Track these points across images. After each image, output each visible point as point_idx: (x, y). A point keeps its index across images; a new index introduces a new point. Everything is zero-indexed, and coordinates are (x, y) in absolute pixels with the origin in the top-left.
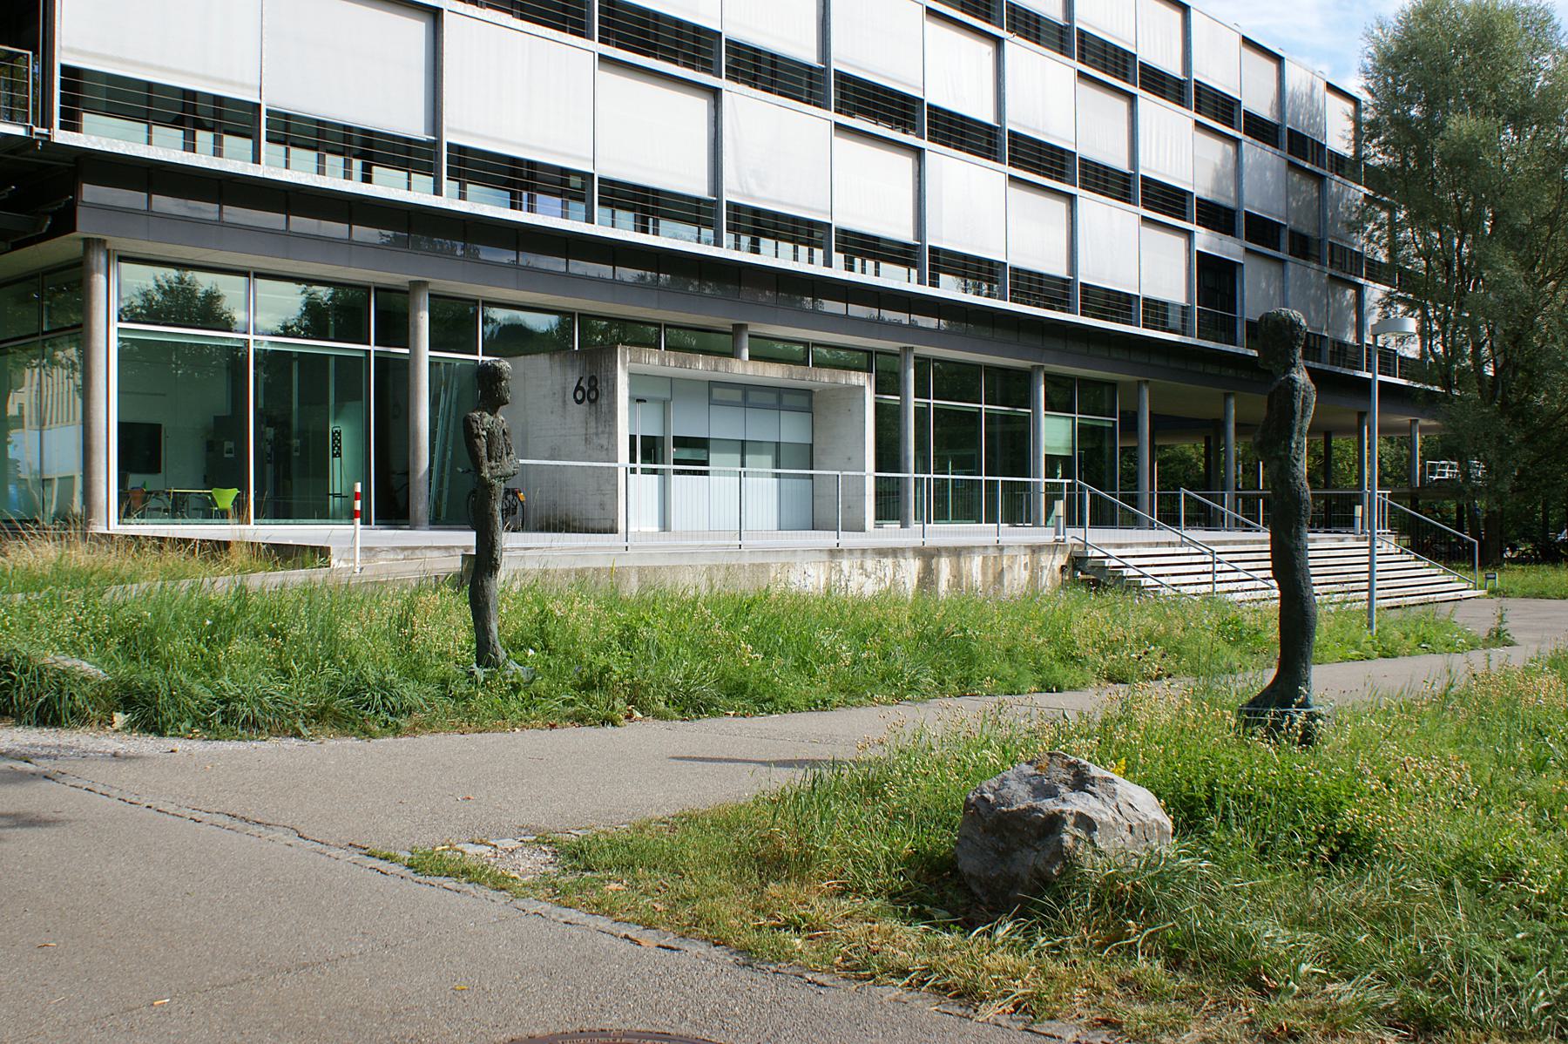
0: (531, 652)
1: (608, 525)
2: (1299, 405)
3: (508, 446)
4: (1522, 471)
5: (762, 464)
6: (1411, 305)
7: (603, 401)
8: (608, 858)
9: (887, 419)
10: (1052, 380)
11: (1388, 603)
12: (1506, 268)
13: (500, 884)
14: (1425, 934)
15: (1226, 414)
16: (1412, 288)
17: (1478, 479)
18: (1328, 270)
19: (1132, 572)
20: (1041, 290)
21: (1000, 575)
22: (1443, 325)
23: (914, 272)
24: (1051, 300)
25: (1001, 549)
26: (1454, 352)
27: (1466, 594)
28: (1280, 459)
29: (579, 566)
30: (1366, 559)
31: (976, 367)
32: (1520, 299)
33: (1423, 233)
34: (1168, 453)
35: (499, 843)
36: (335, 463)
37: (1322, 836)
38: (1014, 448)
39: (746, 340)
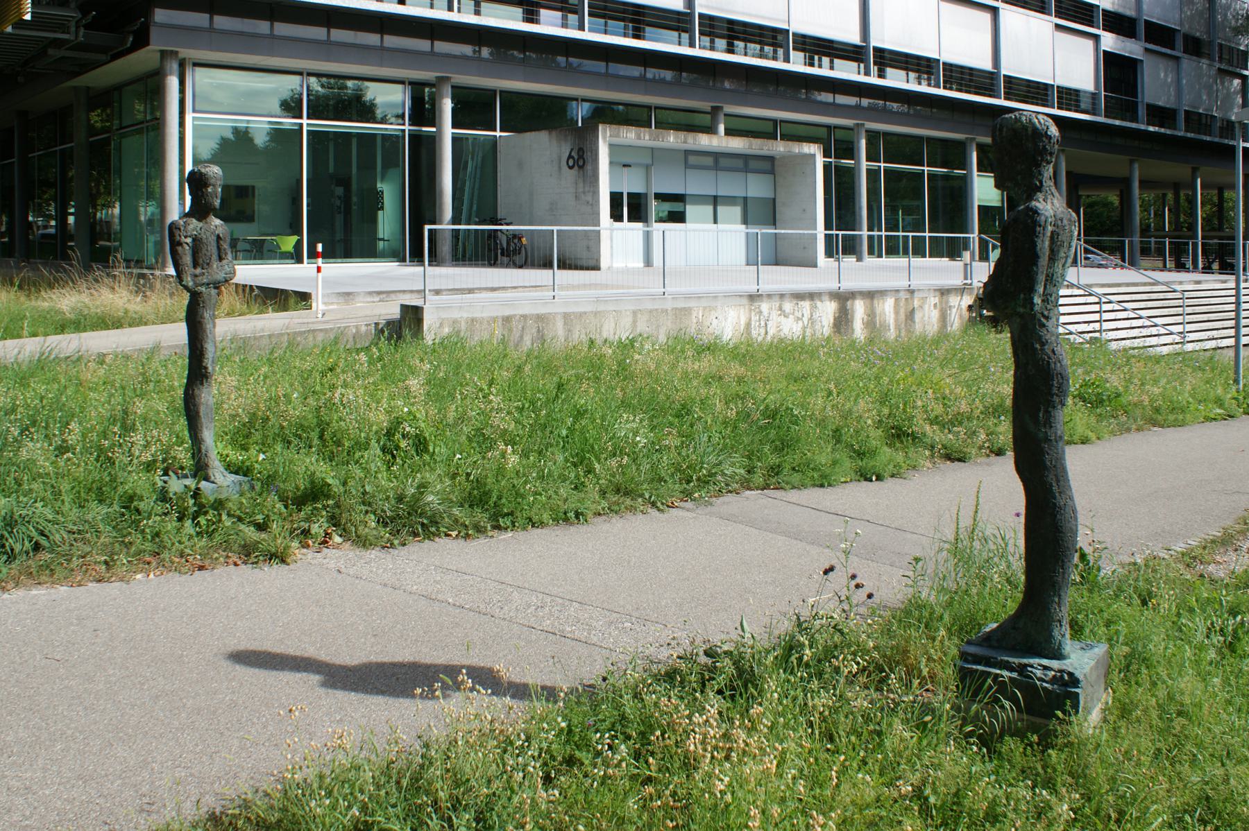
1: (591, 263)
7: (589, 167)
15: (1131, 172)
20: (971, 80)
21: (911, 315)
23: (862, 65)
25: (912, 292)
28: (1021, 316)
29: (507, 313)
39: (722, 117)
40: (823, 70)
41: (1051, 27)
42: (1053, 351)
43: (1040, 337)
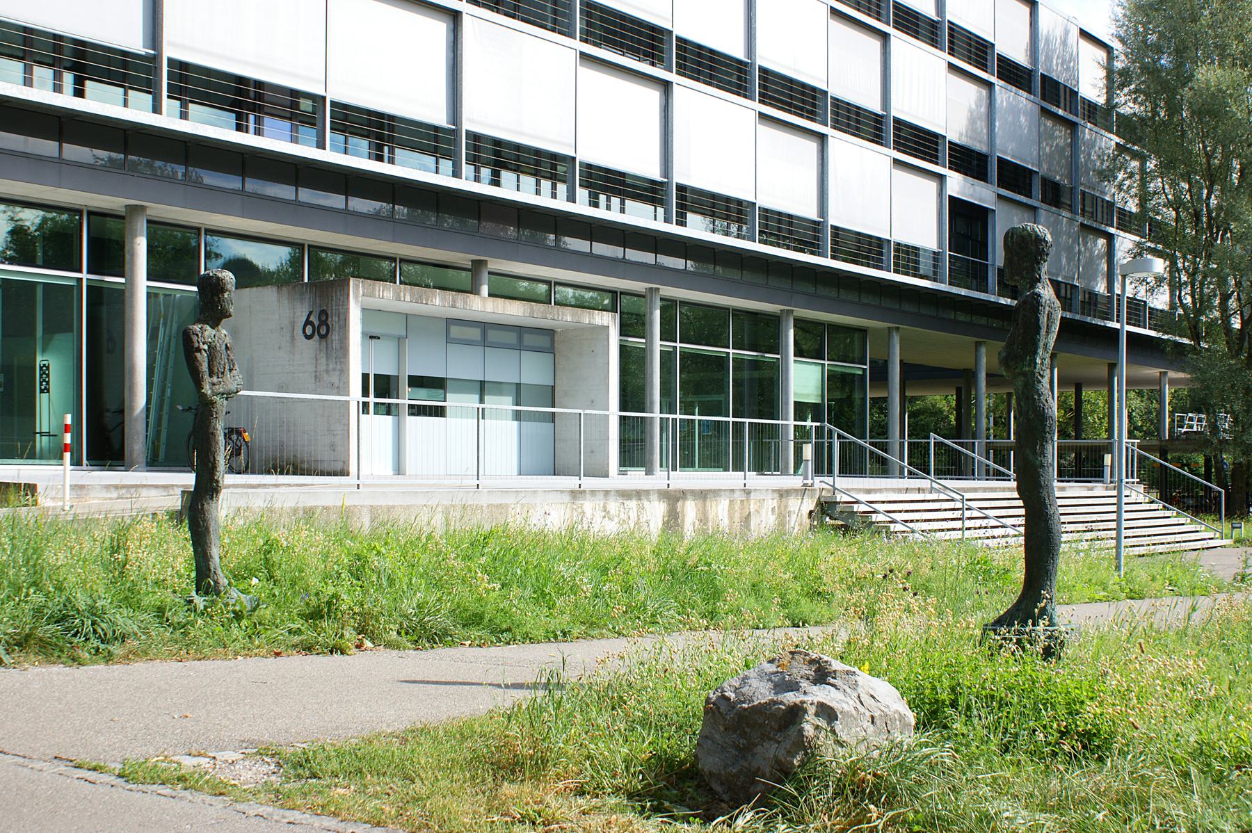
0: (255, 581)
1: (339, 467)
2: (1043, 320)
3: (231, 361)
5: (502, 404)
7: (334, 337)
8: (334, 765)
9: (632, 363)
10: (800, 324)
11: (1137, 551)
13: (219, 790)
14: (1160, 812)
18: (1080, 219)
19: (881, 517)
20: (791, 232)
22: (1192, 275)
23: (660, 211)
24: (800, 242)
25: (748, 492)
26: (1202, 304)
27: (1212, 543)
28: (1025, 374)
31: (725, 309)
33: (1174, 185)
35: (218, 755)
36: (42, 401)
37: (1063, 734)
38: (763, 392)
40: (610, 211)
41: (888, 162)
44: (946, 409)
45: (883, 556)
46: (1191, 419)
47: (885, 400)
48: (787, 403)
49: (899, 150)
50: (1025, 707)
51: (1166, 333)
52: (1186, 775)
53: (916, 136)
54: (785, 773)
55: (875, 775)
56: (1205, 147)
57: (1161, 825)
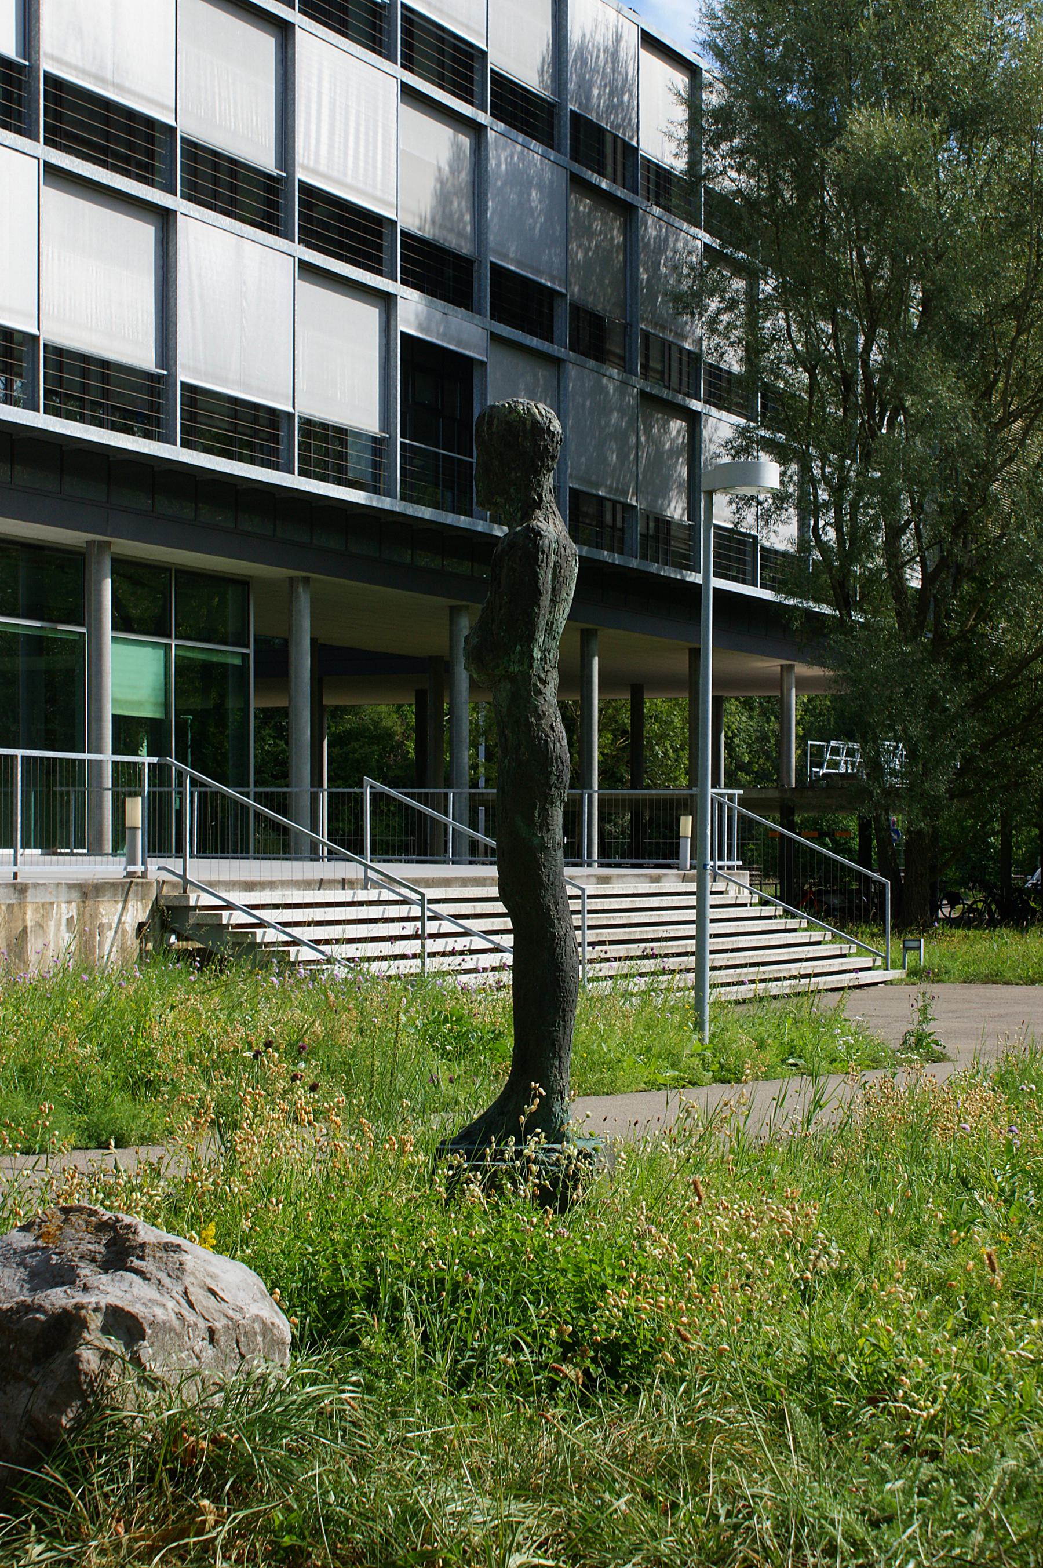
2: (546, 578)
4: (967, 760)
6: (782, 455)
10: (127, 572)
12: (942, 391)
14: (729, 1492)
16: (779, 419)
17: (894, 773)
18: (638, 383)
19: (271, 935)
20: (106, 394)
22: (837, 491)
24: (127, 414)
26: (855, 543)
27: (866, 977)
28: (512, 678)
30: (692, 915)
32: (965, 448)
33: (806, 325)
34: (350, 721)
41: (289, 266)
42: (552, 727)
43: (536, 707)
44: (399, 729)
45: (273, 1012)
46: (835, 751)
47: (284, 712)
48: (99, 719)
49: (309, 245)
50: (498, 1299)
51: (790, 594)
52: (779, 1417)
53: (341, 219)
54: (44, 1442)
55: (215, 1441)
56: (861, 257)
57: (729, 1514)
